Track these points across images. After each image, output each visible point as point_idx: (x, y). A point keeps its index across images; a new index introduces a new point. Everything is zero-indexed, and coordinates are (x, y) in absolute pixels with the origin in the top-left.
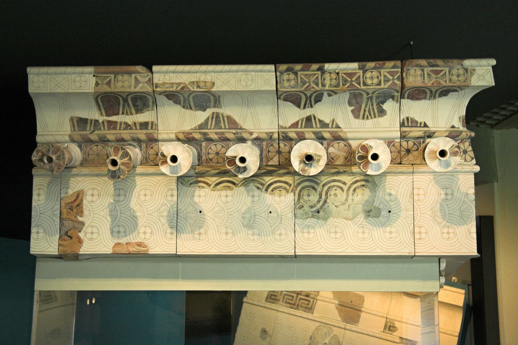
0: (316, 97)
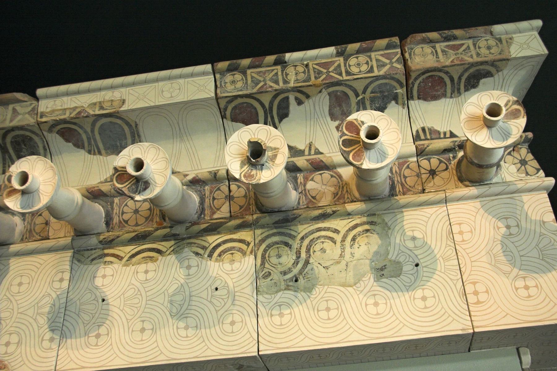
0: (279, 107)
